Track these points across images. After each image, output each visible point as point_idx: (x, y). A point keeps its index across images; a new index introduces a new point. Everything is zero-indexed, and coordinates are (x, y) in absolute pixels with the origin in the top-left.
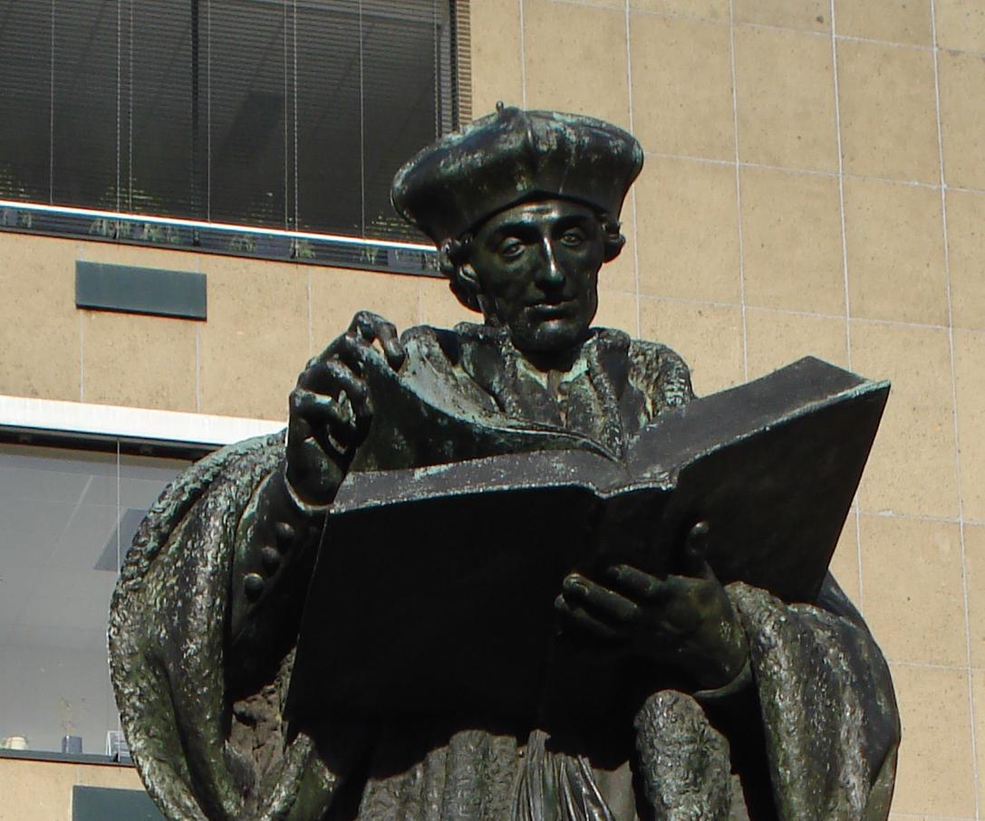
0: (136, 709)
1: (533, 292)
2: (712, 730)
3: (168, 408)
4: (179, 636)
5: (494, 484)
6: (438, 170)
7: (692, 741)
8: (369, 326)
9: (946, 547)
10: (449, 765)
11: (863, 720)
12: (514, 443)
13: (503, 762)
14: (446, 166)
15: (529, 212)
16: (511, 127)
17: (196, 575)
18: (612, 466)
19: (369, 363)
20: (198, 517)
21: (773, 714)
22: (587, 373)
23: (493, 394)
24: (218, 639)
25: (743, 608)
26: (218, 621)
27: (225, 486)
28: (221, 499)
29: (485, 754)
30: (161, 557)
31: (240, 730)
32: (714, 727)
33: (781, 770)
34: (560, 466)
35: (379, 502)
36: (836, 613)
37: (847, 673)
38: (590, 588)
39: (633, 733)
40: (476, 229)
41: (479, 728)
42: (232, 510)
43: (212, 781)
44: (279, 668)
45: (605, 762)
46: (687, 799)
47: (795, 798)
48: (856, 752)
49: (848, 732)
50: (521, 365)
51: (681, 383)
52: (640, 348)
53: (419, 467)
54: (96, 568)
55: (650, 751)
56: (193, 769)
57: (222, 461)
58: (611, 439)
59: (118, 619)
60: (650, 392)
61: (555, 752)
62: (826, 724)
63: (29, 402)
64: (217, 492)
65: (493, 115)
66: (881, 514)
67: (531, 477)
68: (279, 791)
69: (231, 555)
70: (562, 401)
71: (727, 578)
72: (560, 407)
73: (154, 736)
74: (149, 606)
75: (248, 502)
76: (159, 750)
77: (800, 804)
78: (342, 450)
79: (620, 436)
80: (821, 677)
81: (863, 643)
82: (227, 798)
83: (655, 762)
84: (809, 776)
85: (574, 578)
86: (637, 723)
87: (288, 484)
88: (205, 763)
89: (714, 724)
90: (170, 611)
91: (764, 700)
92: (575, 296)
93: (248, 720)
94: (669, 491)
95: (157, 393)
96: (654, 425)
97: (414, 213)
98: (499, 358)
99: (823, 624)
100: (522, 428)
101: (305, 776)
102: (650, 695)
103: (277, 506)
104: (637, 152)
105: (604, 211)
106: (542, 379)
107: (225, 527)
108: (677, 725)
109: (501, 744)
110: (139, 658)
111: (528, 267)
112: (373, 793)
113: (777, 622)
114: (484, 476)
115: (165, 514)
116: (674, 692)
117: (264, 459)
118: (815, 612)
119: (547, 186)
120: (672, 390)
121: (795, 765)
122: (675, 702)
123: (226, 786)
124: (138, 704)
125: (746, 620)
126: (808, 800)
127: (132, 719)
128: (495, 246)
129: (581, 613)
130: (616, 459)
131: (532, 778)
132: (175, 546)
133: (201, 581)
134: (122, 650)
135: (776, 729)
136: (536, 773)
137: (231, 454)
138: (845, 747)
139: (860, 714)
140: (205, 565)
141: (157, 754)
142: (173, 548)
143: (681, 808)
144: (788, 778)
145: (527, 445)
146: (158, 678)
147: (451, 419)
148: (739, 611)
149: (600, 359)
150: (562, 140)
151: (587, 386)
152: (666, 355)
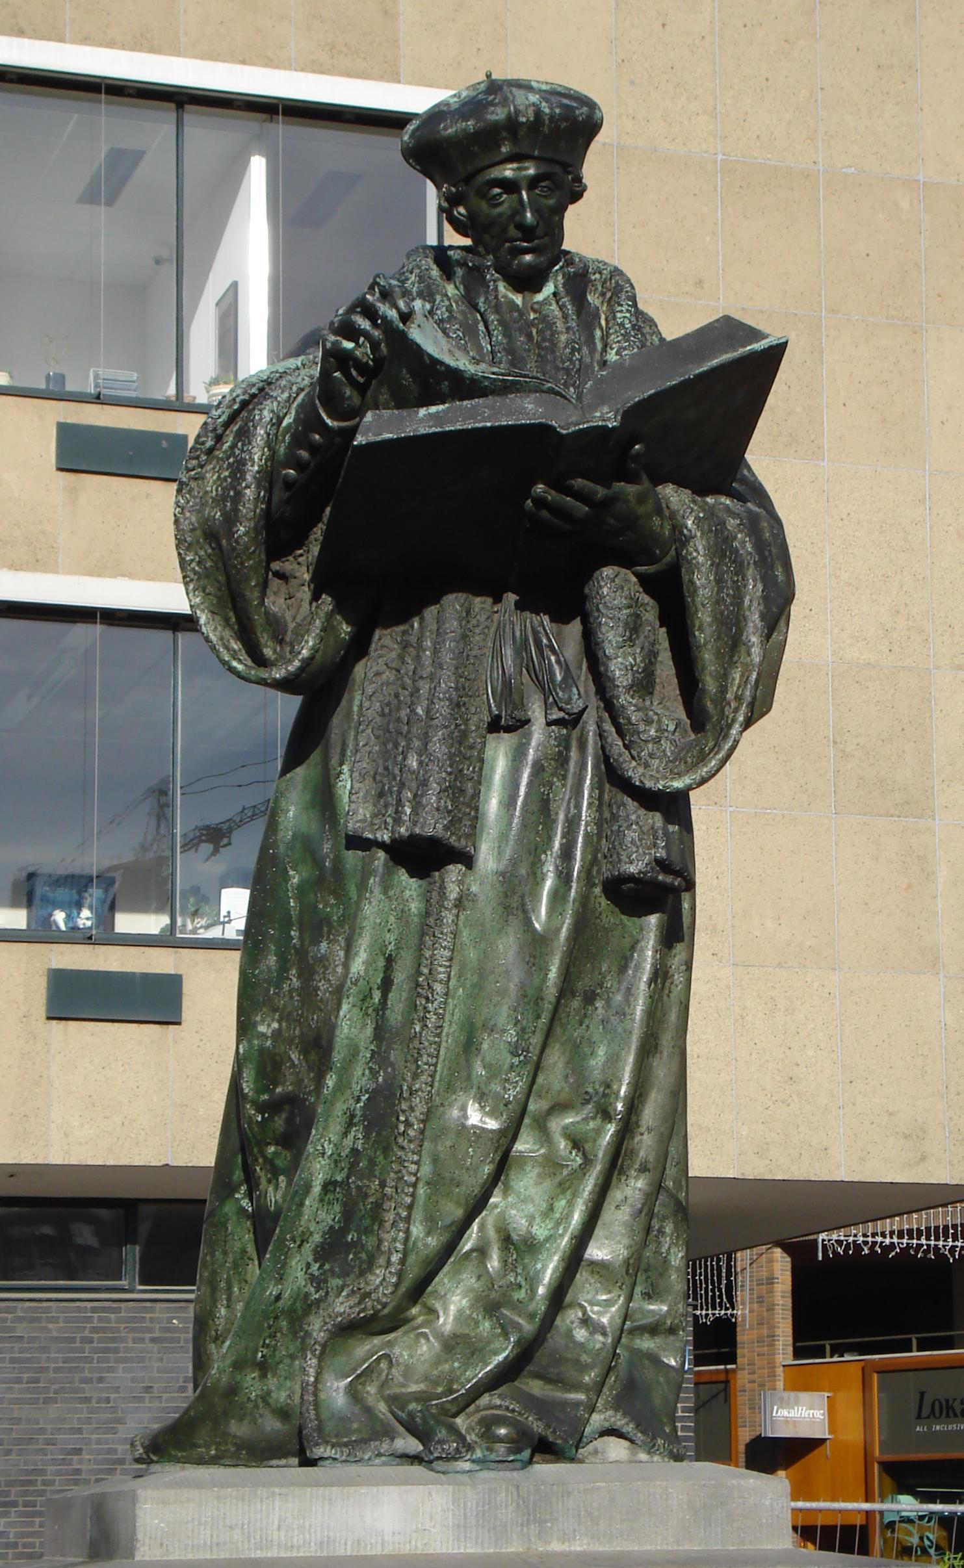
0: (195, 573)
1: (513, 231)
2: (645, 596)
3: (152, 50)
4: (231, 519)
5: (480, 422)
6: (439, 132)
7: (629, 607)
8: (384, 286)
9: (905, 204)
10: (440, 620)
11: (763, 591)
12: (495, 386)
13: (482, 618)
14: (445, 129)
15: (510, 169)
16: (497, 101)
17: (245, 473)
18: (571, 406)
19: (384, 318)
20: (246, 424)
21: (692, 590)
22: (555, 294)
23: (479, 311)
24: (262, 522)
25: (672, 506)
26: (262, 509)
27: (269, 402)
28: (266, 413)
29: (468, 612)
30: (217, 453)
31: (275, 583)
32: (647, 594)
33: (697, 633)
34: (530, 406)
35: (391, 436)
36: (742, 499)
37: (751, 553)
38: (551, 496)
39: (584, 598)
40: (468, 179)
41: (463, 591)
42: (274, 421)
43: (255, 634)
44: (307, 538)
45: (561, 617)
46: (624, 652)
47: (707, 656)
48: (756, 617)
49: (751, 601)
50: (502, 287)
51: (629, 305)
52: (598, 267)
53: (422, 406)
54: (80, 201)
55: (596, 614)
56: (239, 621)
57: (265, 378)
58: (572, 353)
59: (182, 501)
60: (604, 308)
61: (522, 610)
62: (734, 596)
63: (15, 41)
64: (263, 406)
65: (482, 82)
66: (844, 170)
67: (509, 414)
68: (307, 642)
69: (272, 457)
70: (534, 319)
71: (658, 480)
72: (532, 324)
73: (209, 594)
74: (206, 492)
75: (286, 414)
76: (213, 605)
77: (711, 660)
78: (361, 380)
79: (579, 351)
80: (730, 559)
81: (765, 525)
82: (267, 646)
83: (600, 623)
84: (719, 638)
85: (540, 488)
86: (586, 591)
87: (319, 405)
88: (250, 619)
89: (646, 592)
90: (224, 498)
91: (686, 578)
92: (546, 235)
93: (282, 576)
94: (613, 427)
95: (142, 35)
96: (604, 373)
97: (418, 162)
98: (484, 283)
99: (734, 513)
100: (502, 375)
101: (328, 628)
102: (598, 569)
103: (308, 420)
104: (598, 115)
105: (570, 166)
106: (518, 299)
107: (268, 435)
108: (618, 594)
109: (480, 604)
110: (198, 533)
111: (509, 212)
112: (380, 639)
113: (697, 518)
114: (472, 414)
115: (220, 420)
116: (616, 568)
117: (299, 380)
118: (728, 502)
119: (525, 150)
120: (621, 311)
121: (708, 631)
122: (616, 576)
123: (266, 638)
124: (197, 568)
125: (673, 515)
126: (717, 658)
127: (192, 580)
128: (483, 194)
129: (545, 514)
130: (574, 401)
131: (504, 632)
132: (228, 444)
133: (249, 477)
134: (185, 525)
135: (693, 601)
136: (508, 626)
137: (272, 372)
138: (747, 613)
139: (760, 587)
140: (253, 466)
141: (211, 608)
142: (226, 446)
143: (619, 659)
144: (702, 640)
145: (504, 389)
146: (213, 549)
147: (448, 366)
148: (668, 508)
149: (564, 285)
150: (538, 113)
151: (554, 307)
152: (617, 278)
